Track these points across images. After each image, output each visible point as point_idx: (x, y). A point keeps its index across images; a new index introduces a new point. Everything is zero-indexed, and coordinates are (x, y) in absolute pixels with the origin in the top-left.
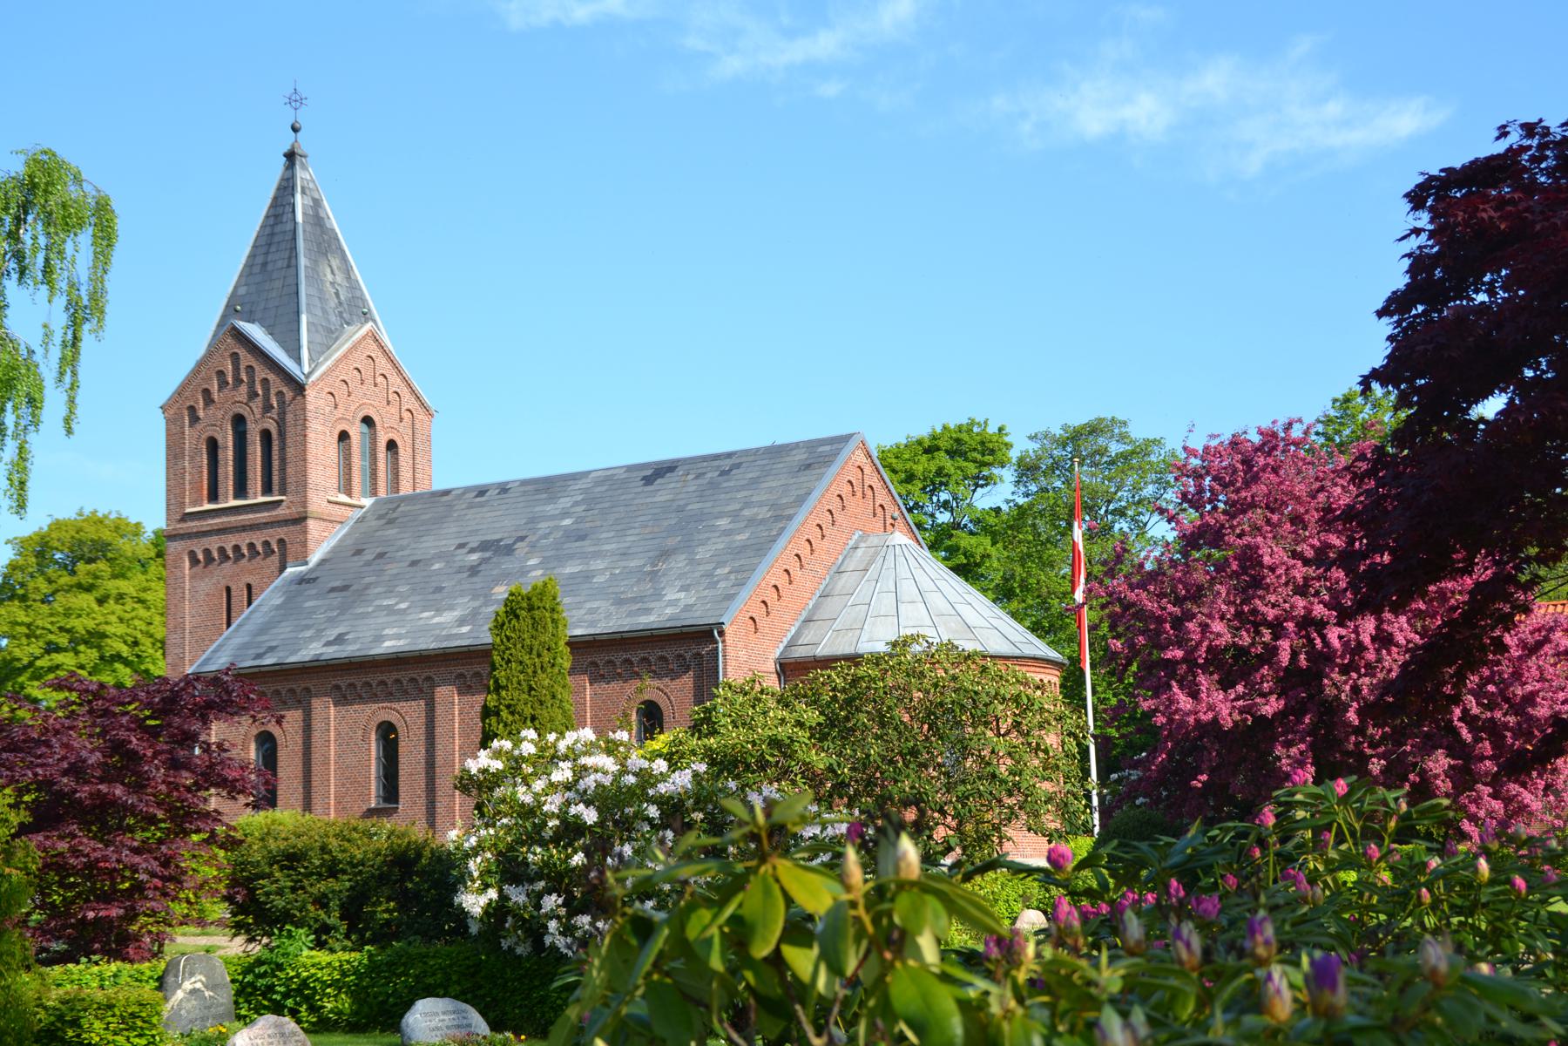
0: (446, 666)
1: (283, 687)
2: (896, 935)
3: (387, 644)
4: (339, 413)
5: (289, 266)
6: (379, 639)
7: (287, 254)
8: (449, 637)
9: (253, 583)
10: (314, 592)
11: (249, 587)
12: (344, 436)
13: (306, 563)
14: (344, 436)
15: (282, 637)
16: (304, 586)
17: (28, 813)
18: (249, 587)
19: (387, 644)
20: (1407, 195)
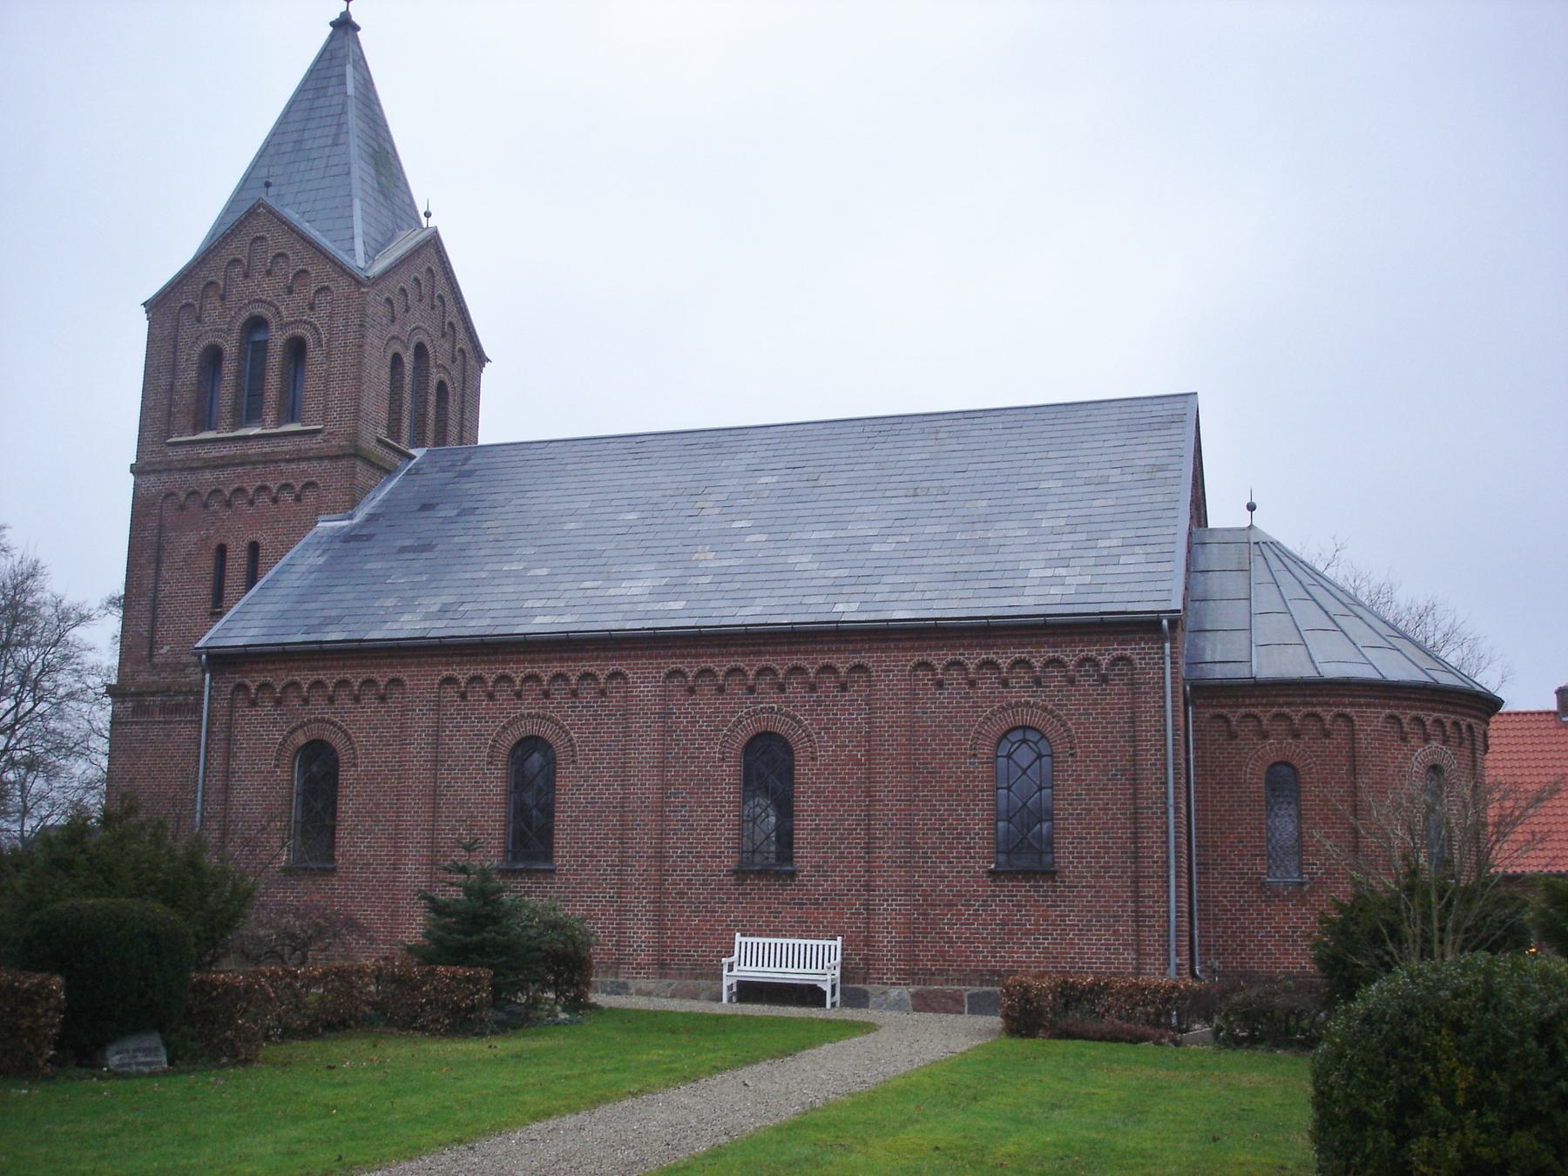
0: (651, 657)
1: (356, 677)
2: (1331, 962)
3: (538, 620)
4: (395, 330)
5: (335, 144)
6: (530, 614)
7: (333, 130)
8: (647, 615)
9: (261, 541)
10: (375, 551)
11: (254, 548)
12: (397, 360)
13: (351, 517)
14: (397, 360)
15: (344, 605)
16: (352, 544)
17: (1455, 1018)
18: (254, 548)
19: (538, 620)
20: (144, 304)
